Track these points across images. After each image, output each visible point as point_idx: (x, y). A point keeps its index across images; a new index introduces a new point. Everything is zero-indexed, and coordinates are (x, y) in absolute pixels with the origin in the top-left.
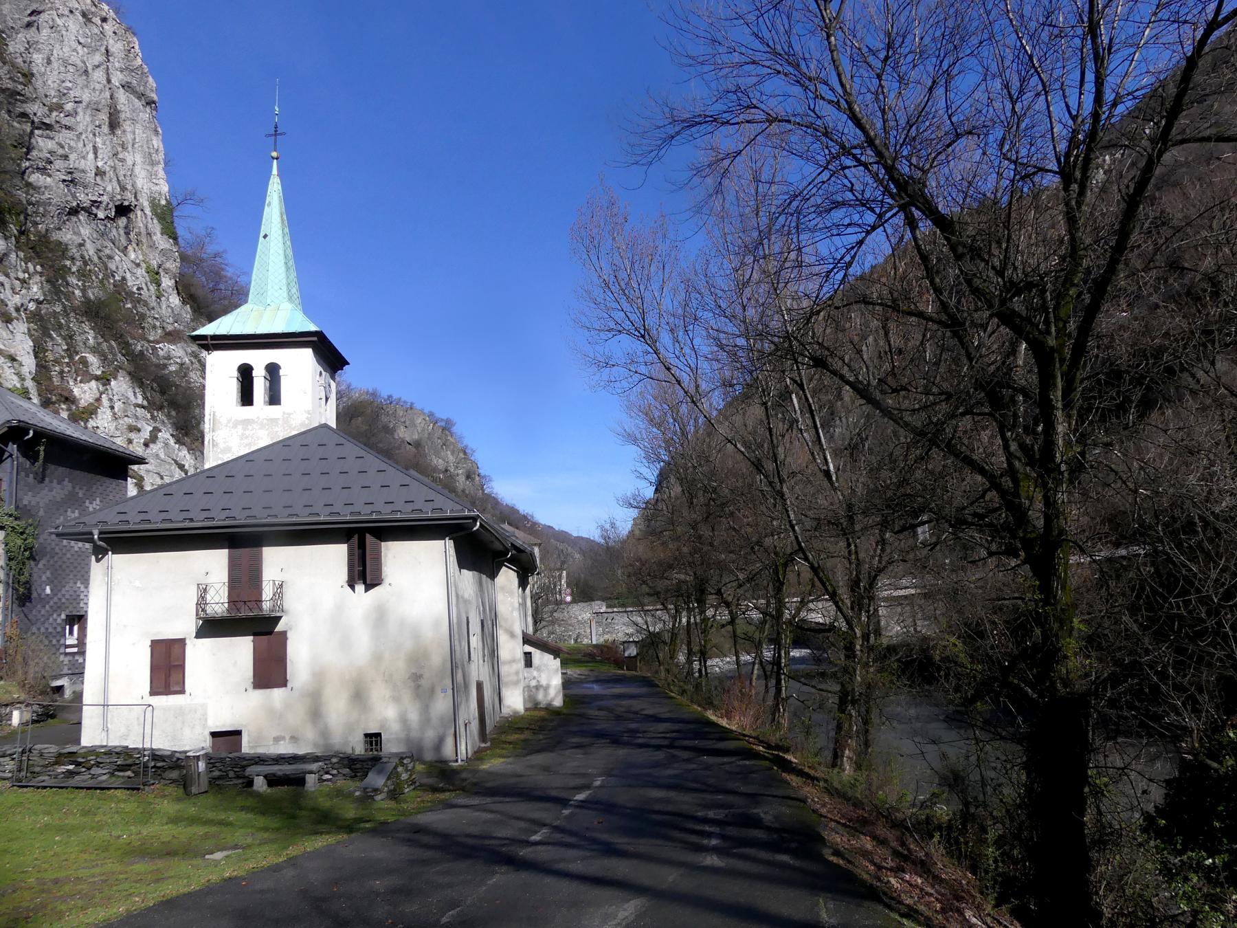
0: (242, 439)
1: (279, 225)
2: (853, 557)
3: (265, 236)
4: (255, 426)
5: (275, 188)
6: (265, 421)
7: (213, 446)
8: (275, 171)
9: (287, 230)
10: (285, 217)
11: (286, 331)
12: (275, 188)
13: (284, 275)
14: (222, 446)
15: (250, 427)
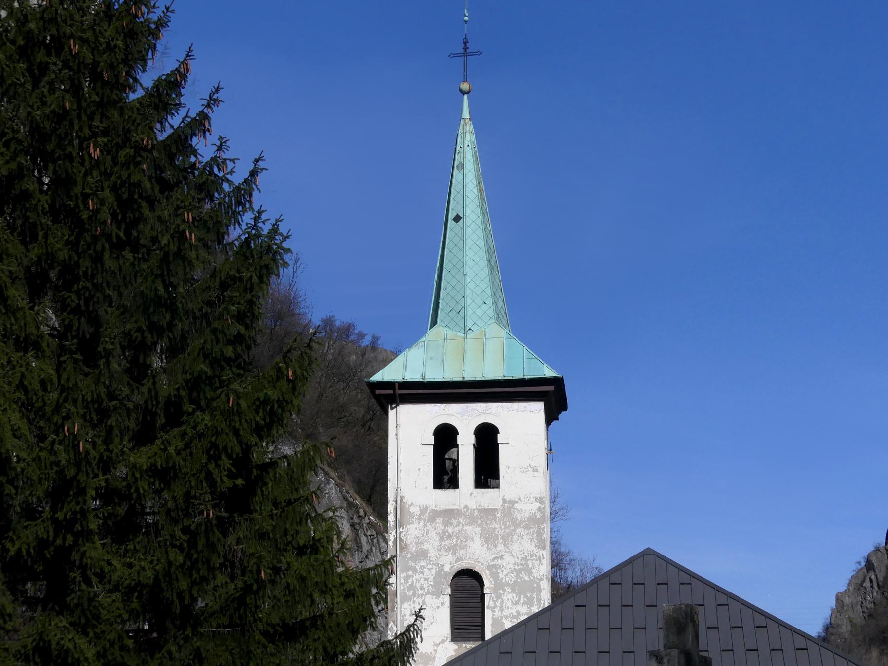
0: (442, 539)
1: (476, 201)
2: (154, 402)
3: (457, 219)
4: (461, 520)
5: (467, 137)
6: (476, 513)
7: (401, 548)
8: (466, 114)
9: (486, 206)
10: (482, 184)
11: (508, 377)
12: (467, 137)
13: (487, 281)
14: (413, 548)
15: (455, 522)
